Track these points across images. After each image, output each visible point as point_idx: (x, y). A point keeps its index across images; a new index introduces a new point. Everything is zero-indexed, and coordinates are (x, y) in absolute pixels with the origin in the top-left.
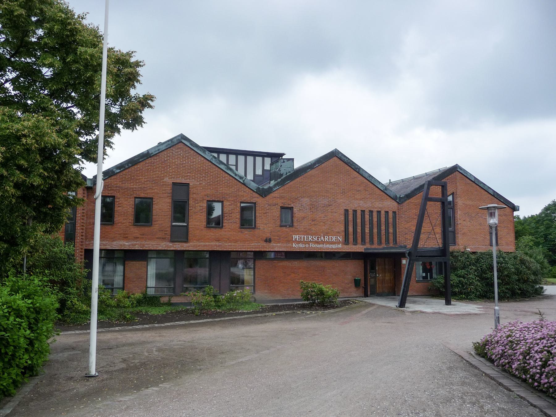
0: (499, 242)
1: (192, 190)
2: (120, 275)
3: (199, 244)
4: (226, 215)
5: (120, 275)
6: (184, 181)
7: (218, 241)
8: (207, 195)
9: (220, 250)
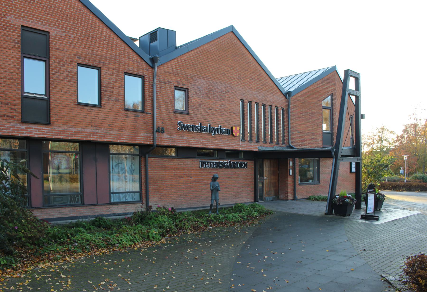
0: (387, 284)
1: (53, 44)
2: (132, 189)
3: (66, 129)
4: (105, 89)
5: (132, 189)
6: (47, 30)
7: (96, 127)
8: (77, 55)
9: (99, 140)
